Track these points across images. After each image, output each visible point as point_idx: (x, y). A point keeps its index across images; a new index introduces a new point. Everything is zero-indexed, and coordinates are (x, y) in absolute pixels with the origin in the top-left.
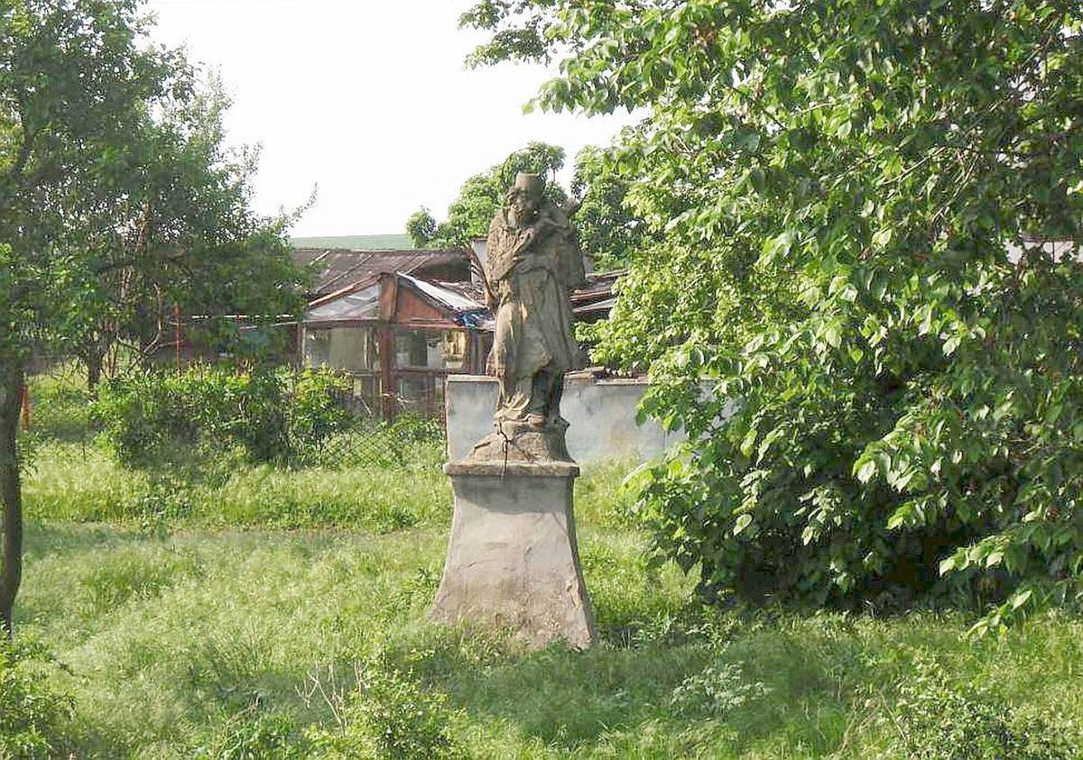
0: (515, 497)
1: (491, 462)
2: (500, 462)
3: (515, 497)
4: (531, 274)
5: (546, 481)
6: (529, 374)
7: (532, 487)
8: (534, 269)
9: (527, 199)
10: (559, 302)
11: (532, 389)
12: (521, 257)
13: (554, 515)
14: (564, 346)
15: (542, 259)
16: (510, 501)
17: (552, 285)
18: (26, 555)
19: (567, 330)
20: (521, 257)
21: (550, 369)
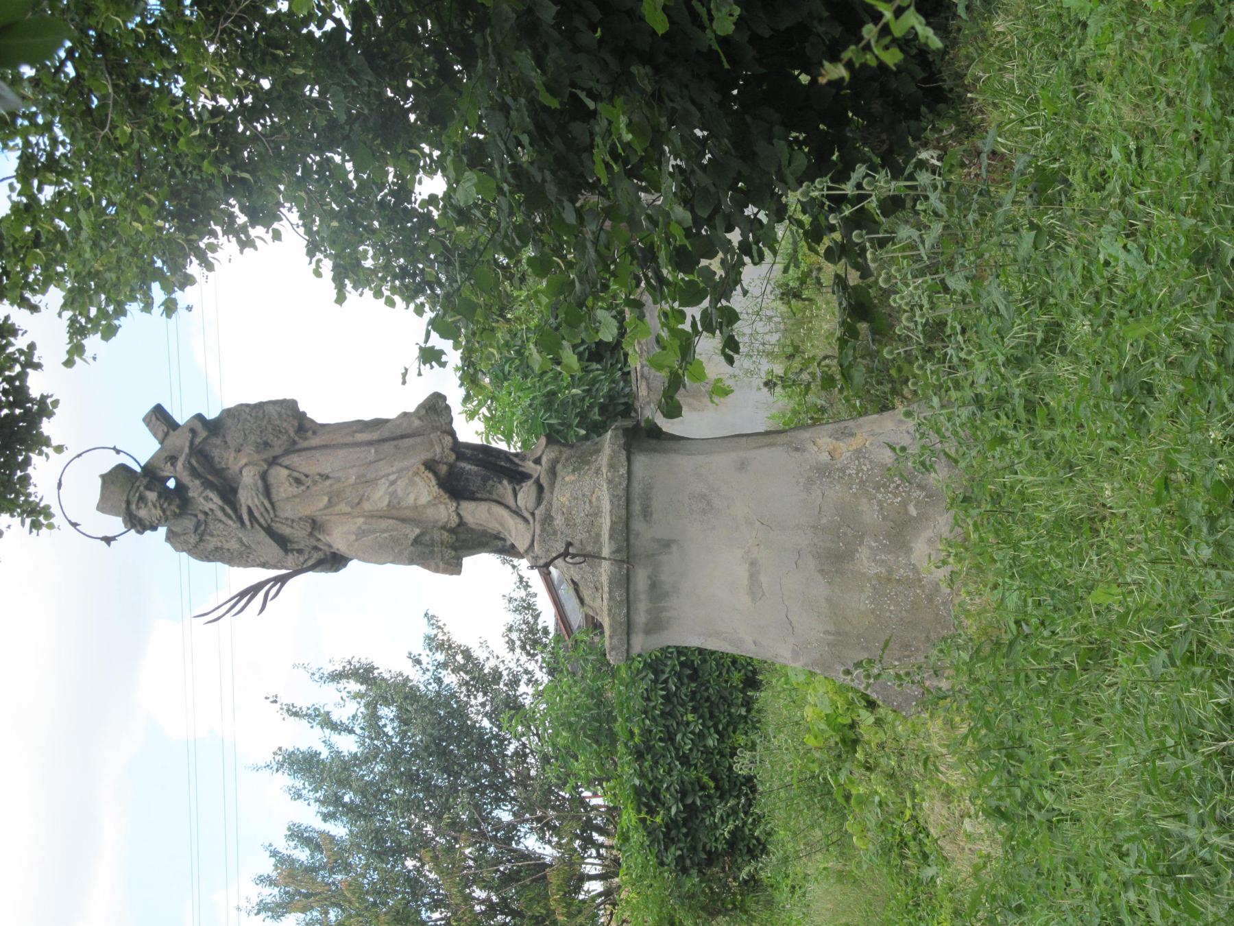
0: (667, 544)
1: (605, 579)
2: (605, 569)
3: (667, 544)
4: (275, 497)
5: (637, 488)
6: (452, 505)
7: (647, 513)
8: (267, 492)
9: (142, 499)
10: (325, 447)
11: (482, 500)
12: (245, 517)
13: (281, 465)
14: (623, 471)
15: (249, 478)
16: (674, 548)
17: (294, 460)
18: (624, 517)
19: (375, 436)
20: (245, 517)
21: (443, 469)
